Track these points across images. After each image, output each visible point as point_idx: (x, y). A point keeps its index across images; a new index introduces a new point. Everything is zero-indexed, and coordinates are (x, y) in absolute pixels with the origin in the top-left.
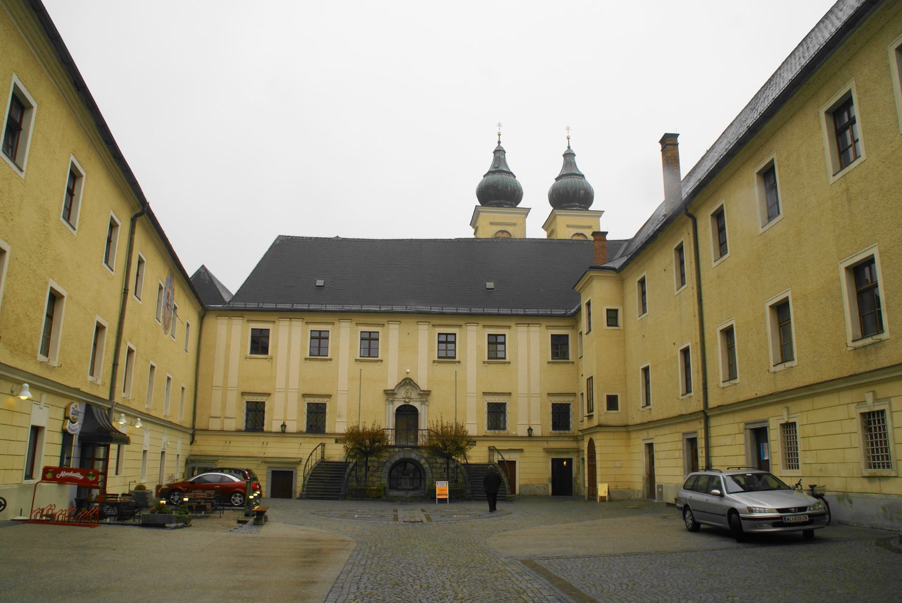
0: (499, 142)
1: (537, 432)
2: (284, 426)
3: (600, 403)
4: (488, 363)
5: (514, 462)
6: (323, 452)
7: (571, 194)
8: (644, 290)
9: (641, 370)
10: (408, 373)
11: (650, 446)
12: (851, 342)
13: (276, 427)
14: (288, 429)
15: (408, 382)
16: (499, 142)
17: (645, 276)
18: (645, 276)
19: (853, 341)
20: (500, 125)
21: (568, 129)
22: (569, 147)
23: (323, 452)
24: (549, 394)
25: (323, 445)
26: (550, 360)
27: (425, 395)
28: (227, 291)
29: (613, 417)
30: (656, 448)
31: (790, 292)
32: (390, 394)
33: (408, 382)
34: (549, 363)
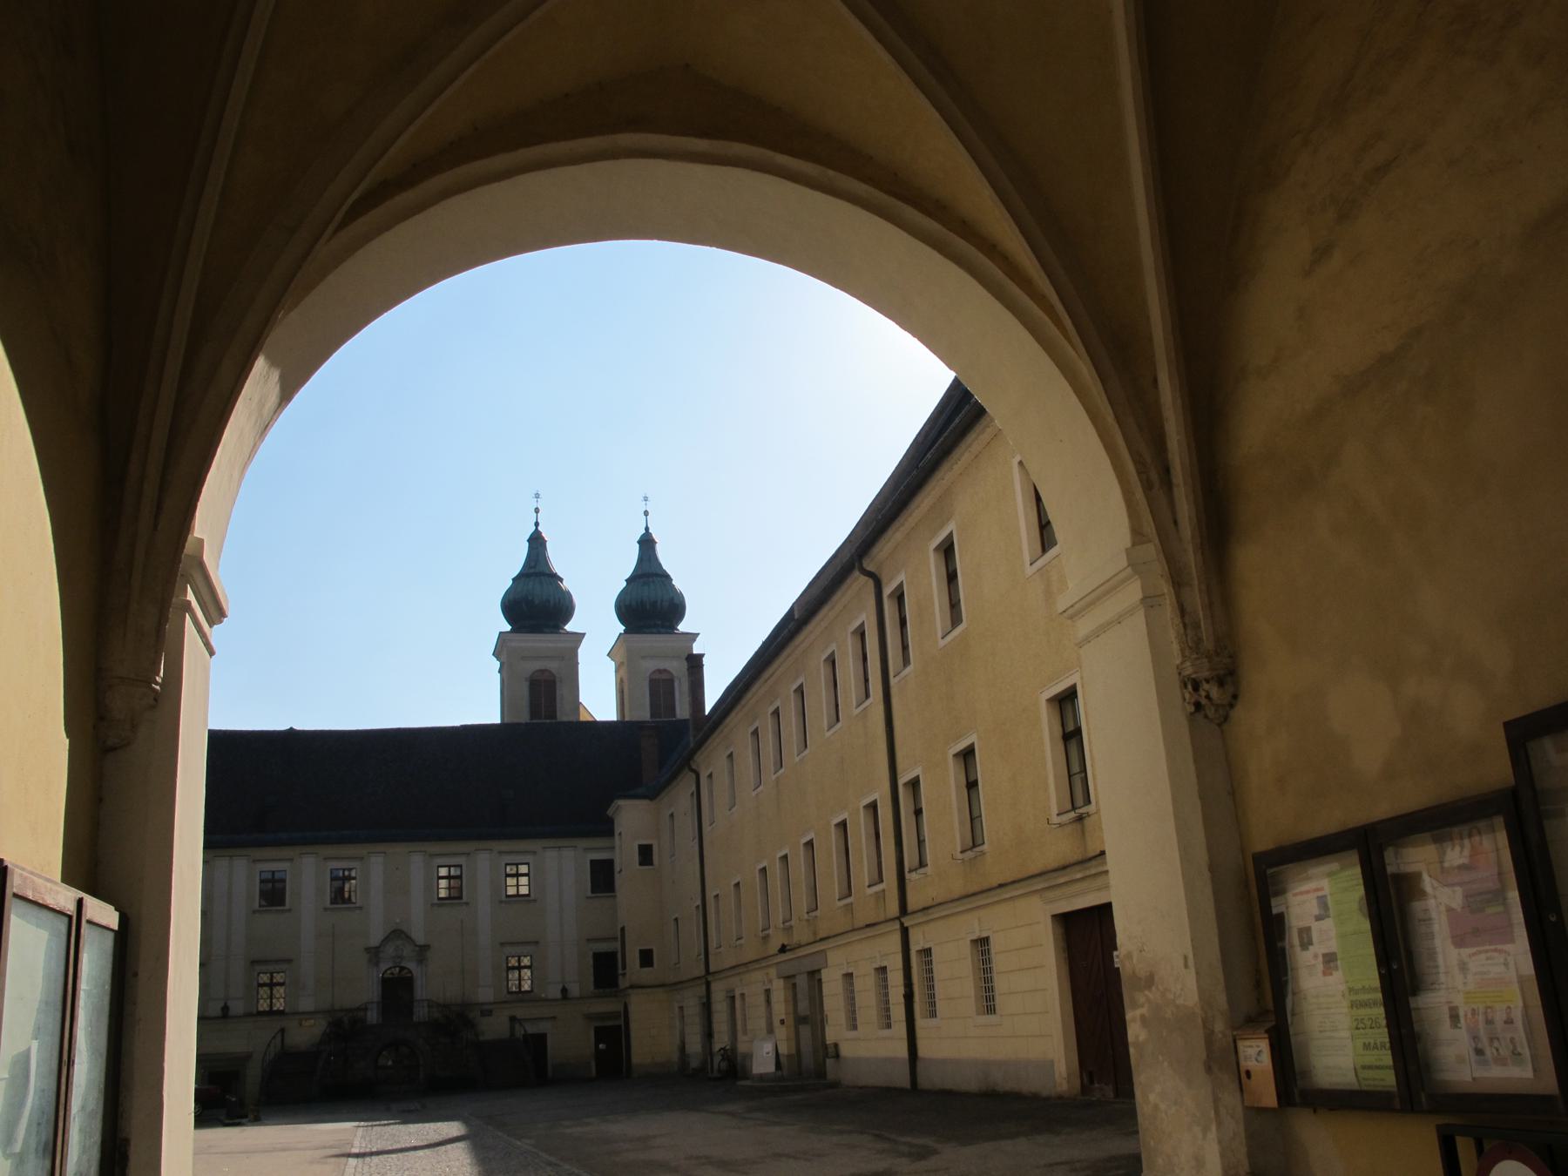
0: (537, 524)
1: (575, 990)
2: (225, 1008)
3: (633, 958)
4: (506, 902)
6: (283, 1040)
7: (648, 607)
8: (903, 616)
9: (833, 829)
11: (982, 943)
12: (1055, 816)
14: (232, 1012)
15: (397, 934)
16: (537, 524)
17: (833, 652)
18: (833, 652)
19: (962, 852)
20: (537, 496)
21: (646, 499)
22: (647, 529)
23: (283, 1040)
24: (588, 940)
25: (282, 1031)
26: (589, 894)
27: (422, 951)
29: (646, 975)
30: (995, 946)
31: (1078, 675)
32: (374, 954)
33: (397, 934)
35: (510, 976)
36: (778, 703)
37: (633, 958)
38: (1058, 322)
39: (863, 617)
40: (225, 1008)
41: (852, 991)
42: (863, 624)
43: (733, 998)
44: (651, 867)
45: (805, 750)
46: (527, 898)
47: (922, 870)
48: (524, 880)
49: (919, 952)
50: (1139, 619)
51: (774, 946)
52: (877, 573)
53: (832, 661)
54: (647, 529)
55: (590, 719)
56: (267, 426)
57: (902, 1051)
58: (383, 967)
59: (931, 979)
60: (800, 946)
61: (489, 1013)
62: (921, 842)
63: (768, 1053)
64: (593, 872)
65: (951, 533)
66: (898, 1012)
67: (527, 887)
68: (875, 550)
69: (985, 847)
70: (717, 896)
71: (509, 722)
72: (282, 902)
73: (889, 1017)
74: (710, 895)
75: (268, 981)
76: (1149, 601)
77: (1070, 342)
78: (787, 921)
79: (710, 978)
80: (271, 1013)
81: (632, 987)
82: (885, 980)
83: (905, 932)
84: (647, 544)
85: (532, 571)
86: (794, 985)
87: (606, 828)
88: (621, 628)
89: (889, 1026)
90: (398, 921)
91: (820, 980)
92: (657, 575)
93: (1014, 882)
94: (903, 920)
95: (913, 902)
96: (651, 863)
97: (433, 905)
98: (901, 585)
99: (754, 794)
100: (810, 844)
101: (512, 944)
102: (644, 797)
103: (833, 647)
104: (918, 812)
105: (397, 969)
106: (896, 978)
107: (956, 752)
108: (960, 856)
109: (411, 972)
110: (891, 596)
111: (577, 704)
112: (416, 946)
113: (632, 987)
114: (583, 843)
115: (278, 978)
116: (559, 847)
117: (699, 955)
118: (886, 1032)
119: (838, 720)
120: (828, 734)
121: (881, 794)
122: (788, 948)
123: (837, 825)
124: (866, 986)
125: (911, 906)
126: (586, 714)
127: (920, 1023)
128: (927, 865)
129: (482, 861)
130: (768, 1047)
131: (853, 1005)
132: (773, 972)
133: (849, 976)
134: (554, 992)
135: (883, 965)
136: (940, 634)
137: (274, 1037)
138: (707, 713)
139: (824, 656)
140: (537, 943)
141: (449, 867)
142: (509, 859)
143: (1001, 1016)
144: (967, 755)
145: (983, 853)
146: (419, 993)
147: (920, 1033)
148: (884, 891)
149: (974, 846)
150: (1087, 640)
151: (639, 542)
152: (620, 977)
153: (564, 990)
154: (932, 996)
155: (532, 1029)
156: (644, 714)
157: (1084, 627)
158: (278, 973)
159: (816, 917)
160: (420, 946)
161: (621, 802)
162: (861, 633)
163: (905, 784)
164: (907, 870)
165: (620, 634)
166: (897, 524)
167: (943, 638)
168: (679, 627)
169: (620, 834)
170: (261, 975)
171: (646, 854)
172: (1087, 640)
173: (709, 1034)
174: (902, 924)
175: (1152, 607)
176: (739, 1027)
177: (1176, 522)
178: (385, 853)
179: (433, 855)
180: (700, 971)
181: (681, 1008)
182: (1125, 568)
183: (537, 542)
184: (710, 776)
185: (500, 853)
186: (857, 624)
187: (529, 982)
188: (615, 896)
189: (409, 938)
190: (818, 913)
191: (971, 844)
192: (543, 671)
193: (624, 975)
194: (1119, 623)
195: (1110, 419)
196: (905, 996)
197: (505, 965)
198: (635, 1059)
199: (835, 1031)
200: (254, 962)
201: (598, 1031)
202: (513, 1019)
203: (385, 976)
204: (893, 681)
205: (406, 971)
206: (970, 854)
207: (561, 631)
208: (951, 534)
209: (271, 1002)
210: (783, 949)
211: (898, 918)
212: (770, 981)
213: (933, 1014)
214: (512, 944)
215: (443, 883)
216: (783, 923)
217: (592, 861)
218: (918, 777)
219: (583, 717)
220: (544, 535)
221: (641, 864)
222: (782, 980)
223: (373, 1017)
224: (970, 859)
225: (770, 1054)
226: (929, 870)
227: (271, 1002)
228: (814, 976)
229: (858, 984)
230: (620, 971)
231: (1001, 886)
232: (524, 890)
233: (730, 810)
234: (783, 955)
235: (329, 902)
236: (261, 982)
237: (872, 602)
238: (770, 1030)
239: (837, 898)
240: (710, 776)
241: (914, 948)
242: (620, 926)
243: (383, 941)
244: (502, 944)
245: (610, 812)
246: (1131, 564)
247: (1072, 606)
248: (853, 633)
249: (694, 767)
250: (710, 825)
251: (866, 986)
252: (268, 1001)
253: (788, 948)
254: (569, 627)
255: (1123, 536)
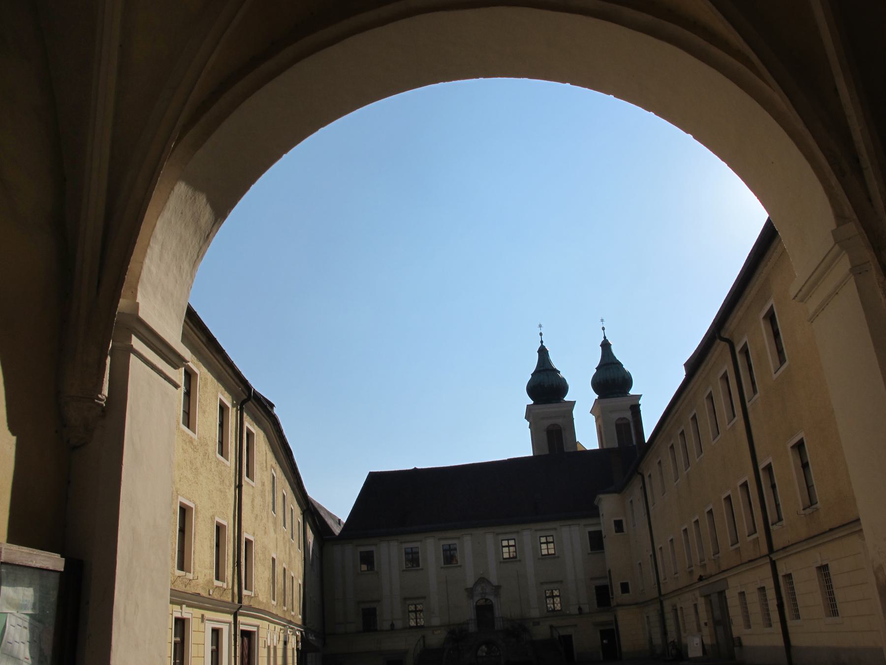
0: (542, 342)
1: (586, 609)
2: (392, 625)
5: (570, 637)
10: (481, 574)
11: (823, 569)
13: (386, 626)
15: (482, 580)
16: (542, 342)
19: (804, 509)
21: (602, 320)
22: (605, 337)
25: (424, 637)
26: (590, 551)
28: (333, 517)
30: (832, 570)
32: (470, 592)
33: (482, 580)
34: (589, 554)
35: (548, 601)
36: (683, 427)
37: (617, 590)
38: (746, 61)
39: (726, 368)
40: (392, 625)
41: (746, 604)
42: (726, 372)
43: (676, 610)
44: (622, 533)
45: (701, 454)
46: (553, 556)
47: (780, 523)
48: (551, 546)
49: (784, 576)
50: (851, 288)
51: (696, 577)
52: (730, 339)
53: (710, 397)
54: (605, 337)
55: (584, 449)
56: (208, 235)
57: (780, 641)
58: (476, 599)
59: (794, 594)
60: (711, 576)
61: (538, 624)
62: (777, 506)
63: (697, 644)
64: (590, 538)
65: (772, 307)
66: (775, 616)
67: (542, 548)
68: (727, 325)
69: (819, 505)
70: (661, 548)
71: (538, 454)
72: (418, 565)
73: (770, 620)
74: (657, 547)
75: (414, 609)
76: (857, 271)
77: (768, 84)
78: (702, 561)
79: (662, 599)
80: (417, 627)
81: (618, 605)
82: (765, 595)
83: (773, 564)
84: (606, 346)
85: (542, 369)
86: (711, 601)
87: (593, 512)
88: (597, 396)
89: (770, 625)
90: (482, 572)
91: (725, 597)
92: (614, 363)
93: (839, 527)
94: (771, 556)
95: (777, 543)
96: (622, 531)
97: (500, 562)
98: (746, 344)
99: (675, 484)
100: (710, 512)
101: (547, 583)
102: (615, 492)
103: (710, 389)
104: (773, 486)
105: (484, 600)
106: (771, 594)
107: (792, 445)
108: (802, 512)
109: (491, 601)
110: (740, 352)
111: (575, 443)
112: (493, 586)
113: (618, 605)
114: (583, 522)
115: (419, 607)
116: (570, 525)
117: (655, 584)
118: (768, 630)
119: (719, 433)
120: (714, 443)
121: (749, 476)
122: (704, 577)
123: (725, 499)
124: (753, 598)
125: (776, 547)
126: (581, 447)
127: (790, 623)
128: (782, 520)
129: (527, 535)
130: (697, 640)
131: (747, 612)
132: (697, 593)
133: (742, 594)
134: (574, 610)
135: (762, 586)
136: (773, 371)
137: (419, 640)
138: (646, 441)
139: (706, 396)
140: (561, 582)
141: (508, 540)
142: (543, 533)
143: (842, 617)
144: (800, 446)
145: (817, 509)
146: (497, 613)
147: (790, 630)
148: (758, 538)
149: (812, 505)
150: (816, 314)
151: (601, 346)
152: (611, 600)
153: (580, 609)
154: (796, 605)
155: (563, 632)
156: (615, 444)
157: (813, 304)
158: (419, 604)
159: (719, 557)
160: (495, 586)
161: (601, 496)
162: (725, 377)
163: (764, 469)
164: (770, 523)
165: (596, 400)
166: (738, 306)
167: (775, 373)
168: (630, 392)
169: (603, 515)
170: (410, 606)
171: (619, 526)
172: (816, 314)
173: (665, 633)
174: (771, 559)
175: (860, 273)
176: (682, 628)
177: (870, 200)
178: (471, 534)
179: (498, 534)
180: (656, 595)
181: (648, 617)
182: (833, 248)
183: (543, 352)
184: (650, 476)
185: (536, 530)
186: (722, 373)
187: (559, 605)
188: (604, 552)
189: (489, 582)
190: (719, 555)
191: (809, 504)
192: (554, 425)
193: (613, 598)
194: (837, 293)
195: (800, 125)
196: (778, 605)
197: (544, 596)
198: (624, 649)
199: (737, 629)
200: (405, 599)
201: (602, 632)
202: (551, 627)
203: (478, 604)
204: (748, 405)
205: (489, 601)
206: (809, 511)
207: (562, 401)
208: (772, 307)
209: (416, 621)
210: (701, 579)
211: (768, 555)
212: (697, 599)
213: (798, 617)
214: (547, 583)
215: (506, 550)
216: (700, 562)
217: (590, 533)
218: (770, 463)
219: (579, 449)
220: (546, 347)
221: (616, 532)
222: (703, 598)
223: (472, 628)
224: (810, 514)
225: (699, 645)
226: (784, 522)
227: (416, 621)
228: (722, 594)
229: (749, 598)
230: (611, 597)
231: (831, 530)
232: (552, 551)
233: (663, 495)
234: (701, 582)
235: (443, 564)
236: (410, 610)
237: (729, 357)
238: (700, 630)
239: (730, 544)
240: (650, 476)
241: (781, 574)
242: (608, 570)
243: (474, 585)
244: (542, 583)
245: (596, 503)
246: (837, 242)
247: (800, 290)
248: (721, 378)
249: (640, 471)
250: (653, 506)
251: (753, 598)
252: (415, 620)
253: (704, 577)
254: (566, 399)
255: (829, 220)
